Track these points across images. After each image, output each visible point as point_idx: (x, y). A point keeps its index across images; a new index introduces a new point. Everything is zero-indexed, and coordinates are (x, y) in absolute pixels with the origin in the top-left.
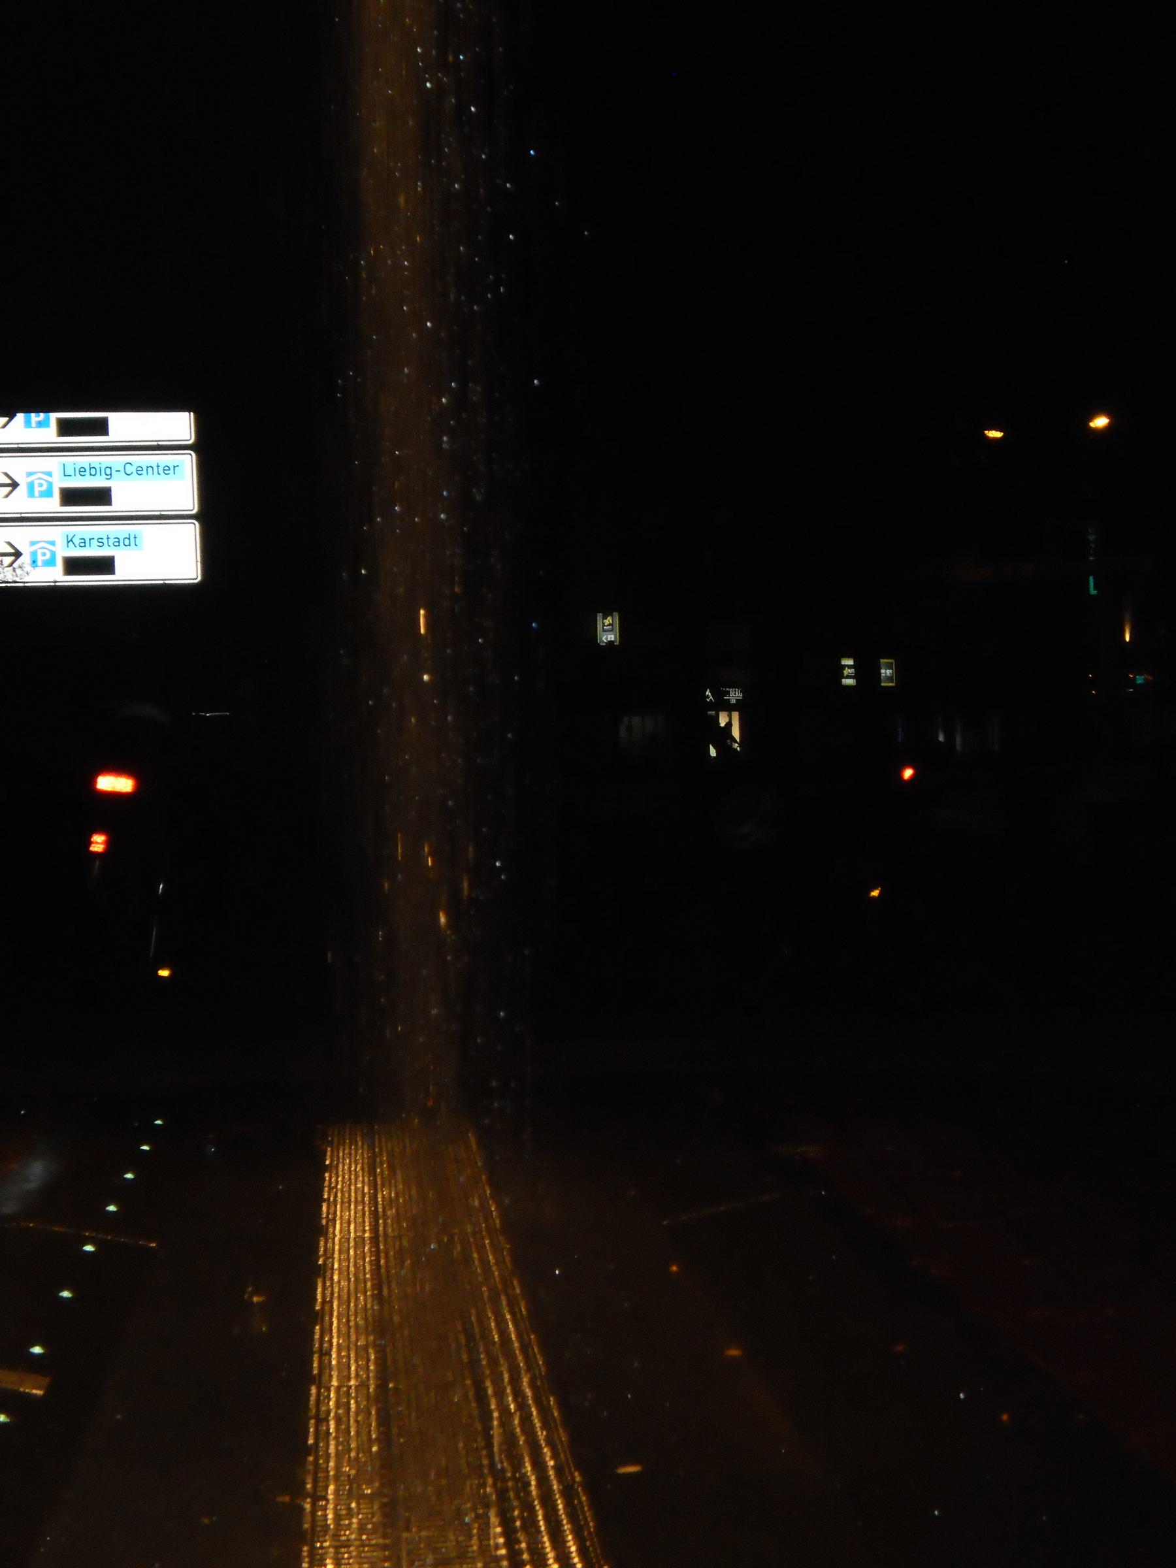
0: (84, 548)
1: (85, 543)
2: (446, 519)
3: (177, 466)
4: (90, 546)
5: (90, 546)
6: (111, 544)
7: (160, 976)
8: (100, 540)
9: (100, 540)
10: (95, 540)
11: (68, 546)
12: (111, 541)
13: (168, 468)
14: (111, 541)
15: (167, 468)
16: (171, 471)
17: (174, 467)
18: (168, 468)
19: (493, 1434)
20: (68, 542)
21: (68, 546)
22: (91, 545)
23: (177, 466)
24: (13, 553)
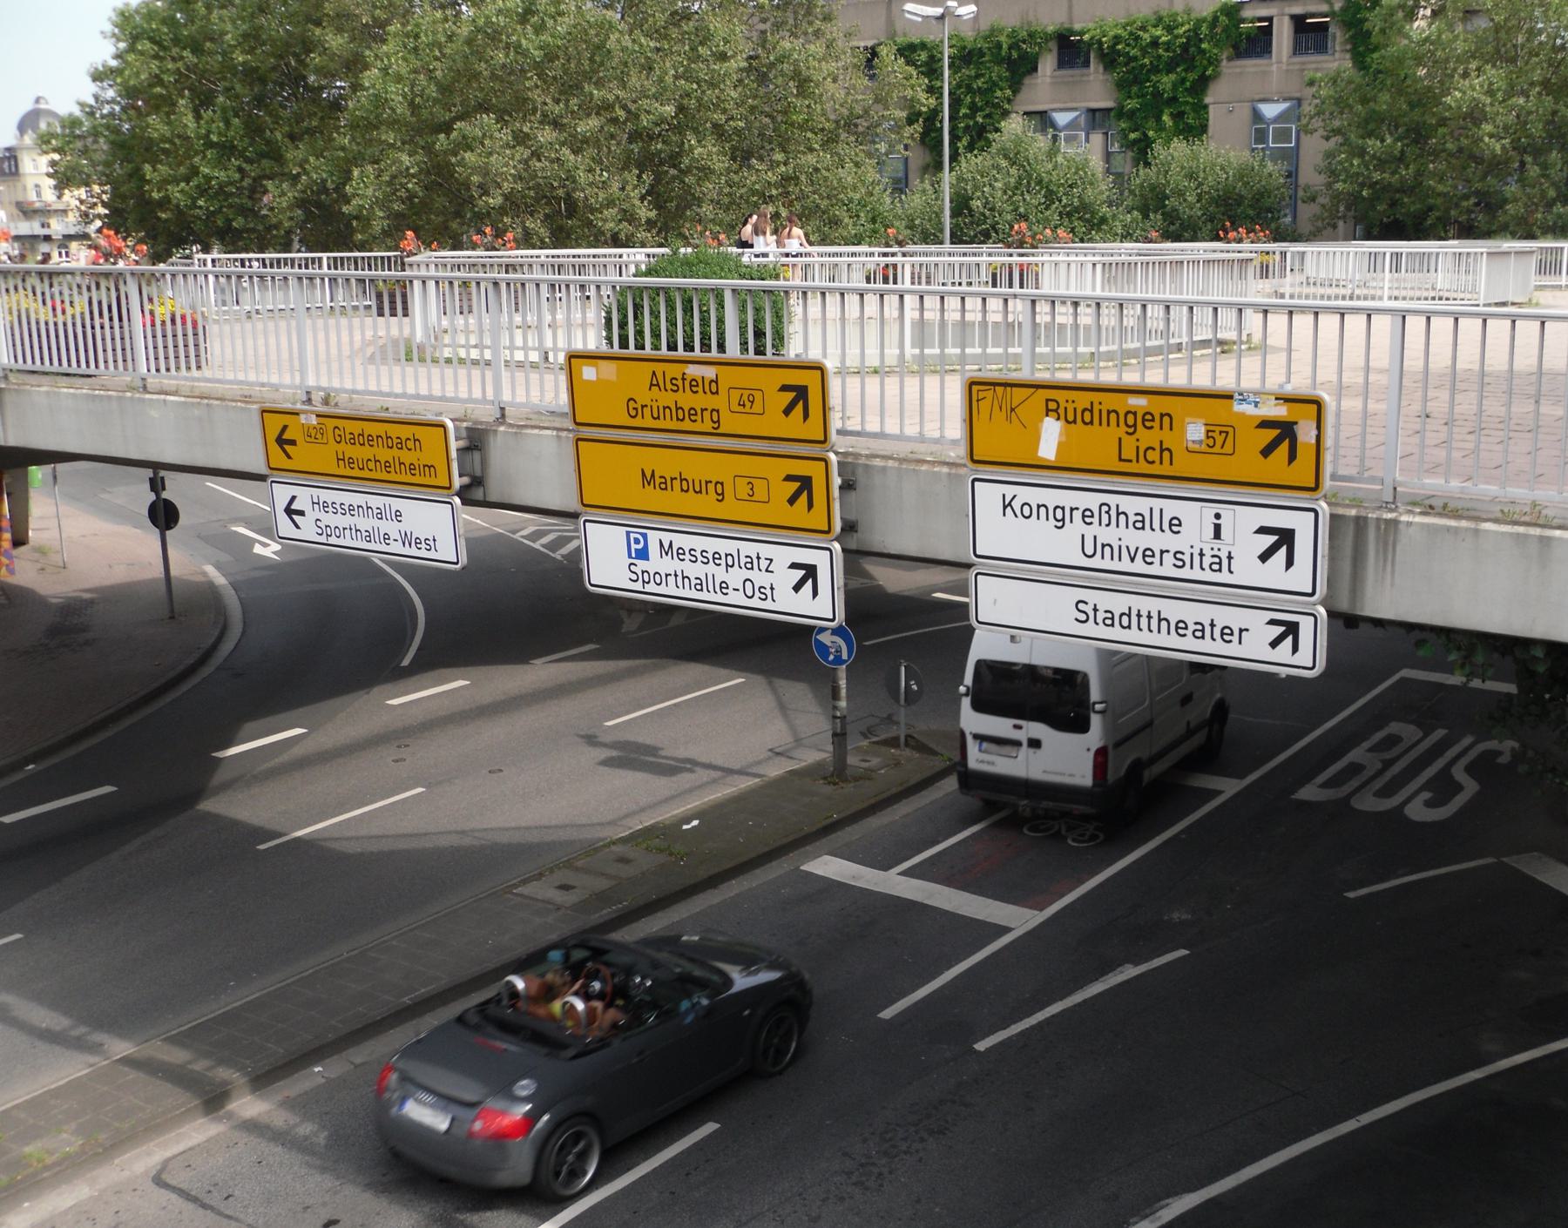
0: (1141, 531)
1: (1143, 522)
2: (601, 982)
3: (1247, 630)
4: (1120, 560)
5: (1120, 560)
6: (1099, 620)
7: (1480, 784)
8: (1178, 556)
9: (1178, 556)
10: (1171, 554)
11: (1004, 515)
12: (1101, 616)
13: (1150, 417)
14: (1101, 616)
15: (1148, 417)
16: (1235, 638)
17: (1241, 631)
18: (1150, 417)
19: (698, 814)
20: (1005, 507)
21: (1004, 515)
22: (1392, 490)
23: (1247, 630)
24: (800, 487)
